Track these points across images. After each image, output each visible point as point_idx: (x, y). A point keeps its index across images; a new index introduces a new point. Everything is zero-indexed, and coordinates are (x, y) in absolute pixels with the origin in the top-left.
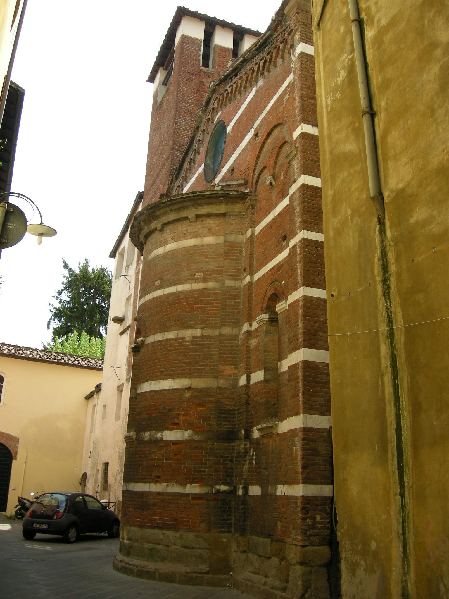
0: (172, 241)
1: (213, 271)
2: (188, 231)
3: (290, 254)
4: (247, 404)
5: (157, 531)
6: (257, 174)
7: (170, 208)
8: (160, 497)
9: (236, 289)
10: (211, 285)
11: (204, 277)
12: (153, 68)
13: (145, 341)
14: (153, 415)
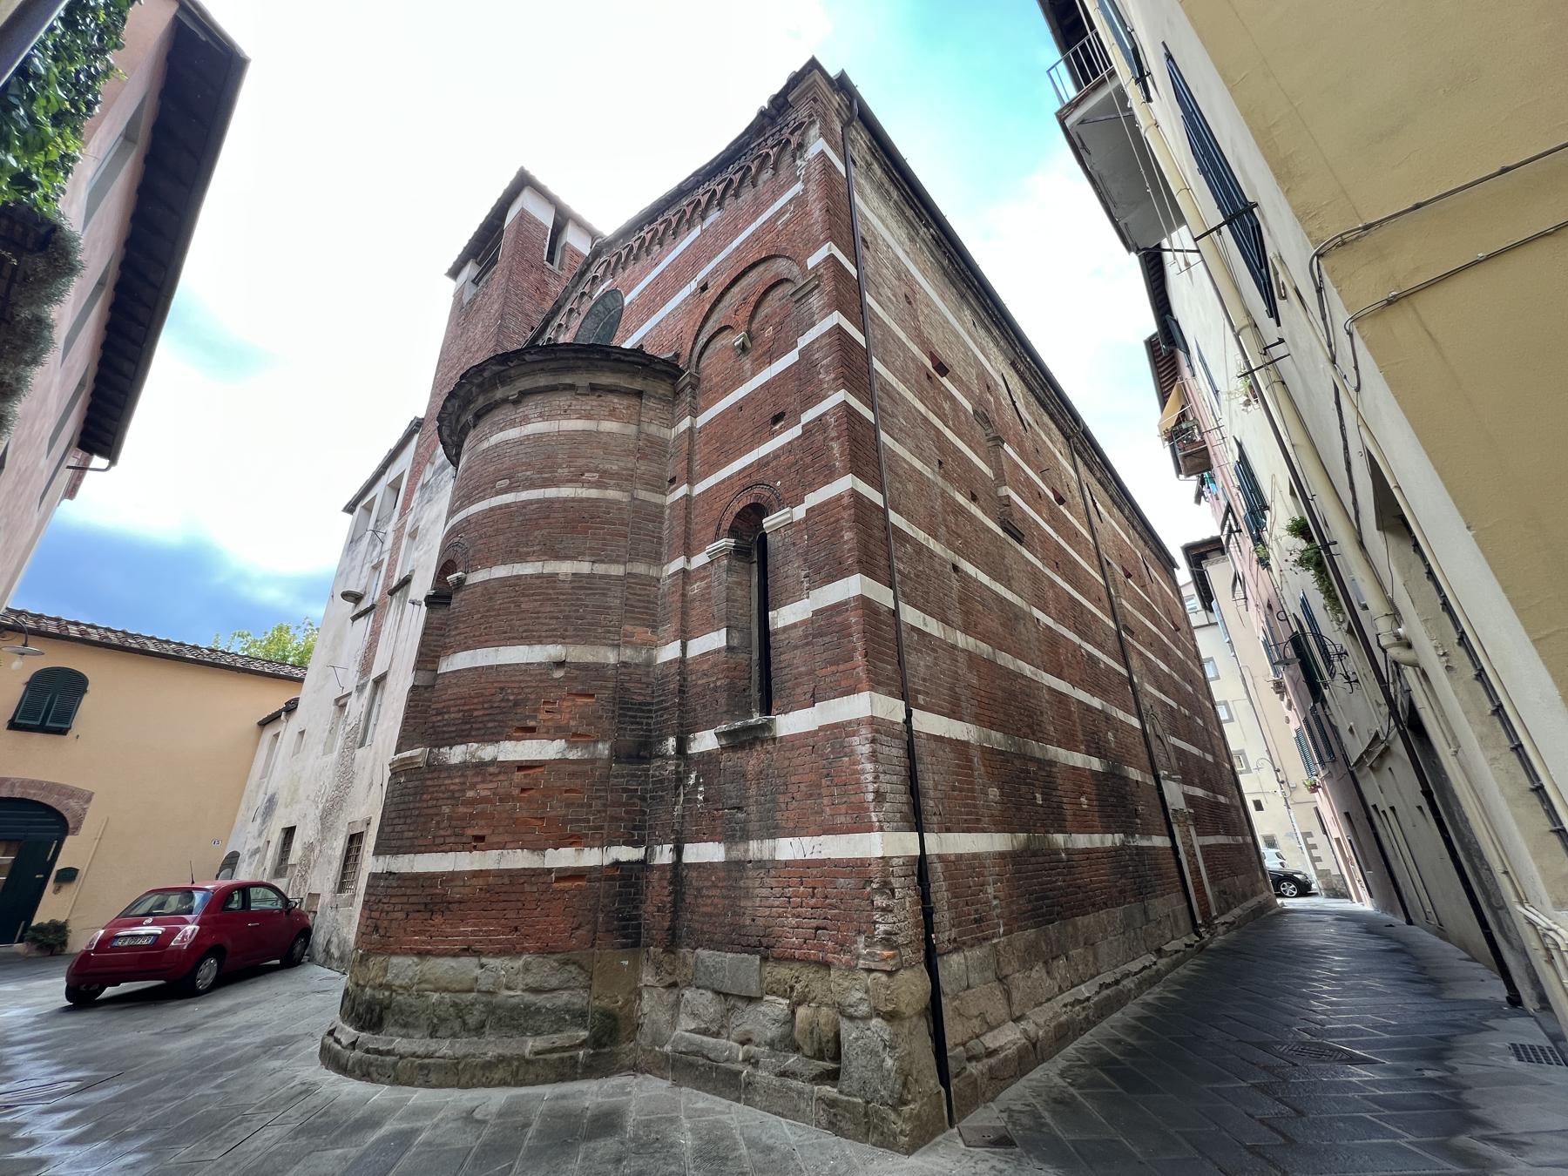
4: (682, 691)
5: (468, 963)
6: (703, 339)
8: (480, 882)
9: (656, 505)
10: (612, 494)
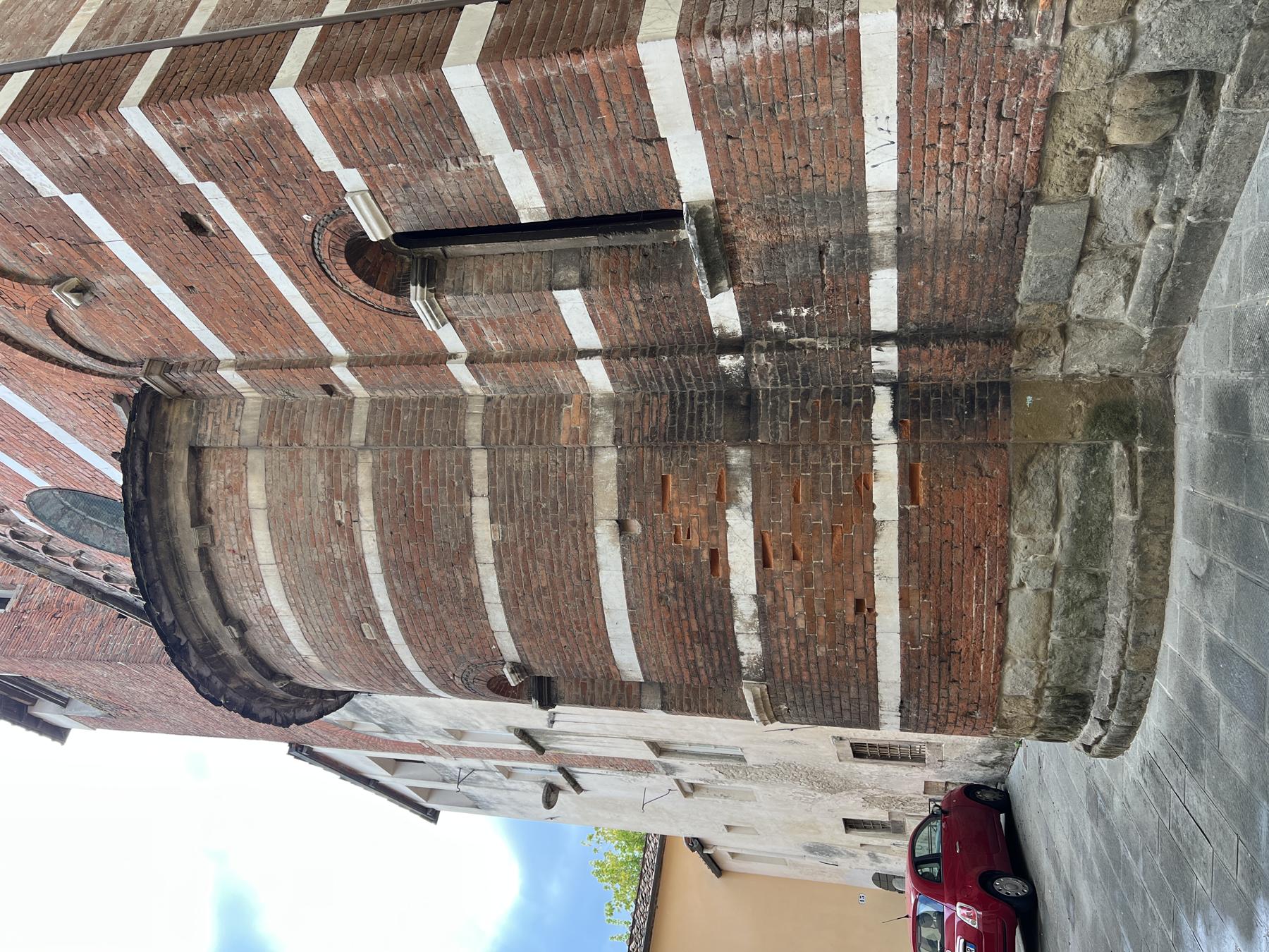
0: (262, 592)
1: (330, 475)
2: (235, 547)
3: (212, 178)
5: (1016, 603)
7: (178, 600)
8: (915, 599)
9: (372, 412)
10: (364, 479)
11: (346, 499)
12: (28, 728)
13: (513, 663)
14: (695, 628)
